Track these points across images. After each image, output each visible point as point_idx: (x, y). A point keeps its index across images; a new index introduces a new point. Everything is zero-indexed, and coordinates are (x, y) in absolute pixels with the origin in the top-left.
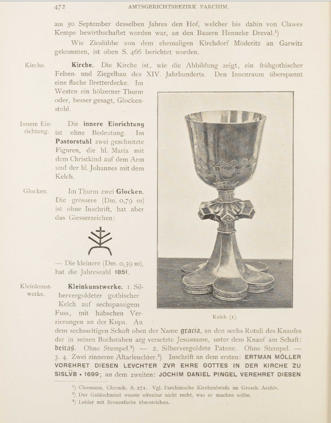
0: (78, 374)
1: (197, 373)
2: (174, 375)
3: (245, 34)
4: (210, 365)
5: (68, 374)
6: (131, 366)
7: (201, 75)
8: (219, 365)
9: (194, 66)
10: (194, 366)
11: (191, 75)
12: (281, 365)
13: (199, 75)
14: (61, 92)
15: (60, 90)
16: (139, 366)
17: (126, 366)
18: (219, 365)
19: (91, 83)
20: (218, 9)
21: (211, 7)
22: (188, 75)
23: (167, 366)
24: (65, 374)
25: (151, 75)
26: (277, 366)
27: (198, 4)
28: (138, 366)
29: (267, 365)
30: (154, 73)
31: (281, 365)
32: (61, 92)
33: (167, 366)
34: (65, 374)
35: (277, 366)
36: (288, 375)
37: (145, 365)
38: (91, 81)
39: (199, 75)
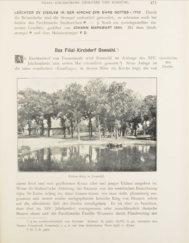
0: (129, 12)
1: (63, 12)
2: (25, 13)
3: (129, 18)
4: (118, 12)
5: (53, 12)
6: (19, 13)
7: (48, 64)
8: (124, 12)
9: (62, 189)
10: (110, 13)
11: (42, 64)
12: (87, 12)
13: (47, 64)
14: (20, 189)
15: (100, 213)
16: (24, 13)
17: (16, 13)
18: (28, 12)
19: (137, 189)
20: (64, 4)
21: (61, 3)
22: (63, 69)
23: (94, 13)
24: (51, 12)
25: (47, 209)
26: (84, 12)
27: (53, 2)
28: (23, 13)
29: (79, 12)
30: (49, 208)
31: (106, 12)
32: (20, 189)
33: (94, 13)
34: (51, 12)
35: (84, 12)
36: (126, 12)
37: (27, 12)
38: (137, 188)
39: (47, 64)
